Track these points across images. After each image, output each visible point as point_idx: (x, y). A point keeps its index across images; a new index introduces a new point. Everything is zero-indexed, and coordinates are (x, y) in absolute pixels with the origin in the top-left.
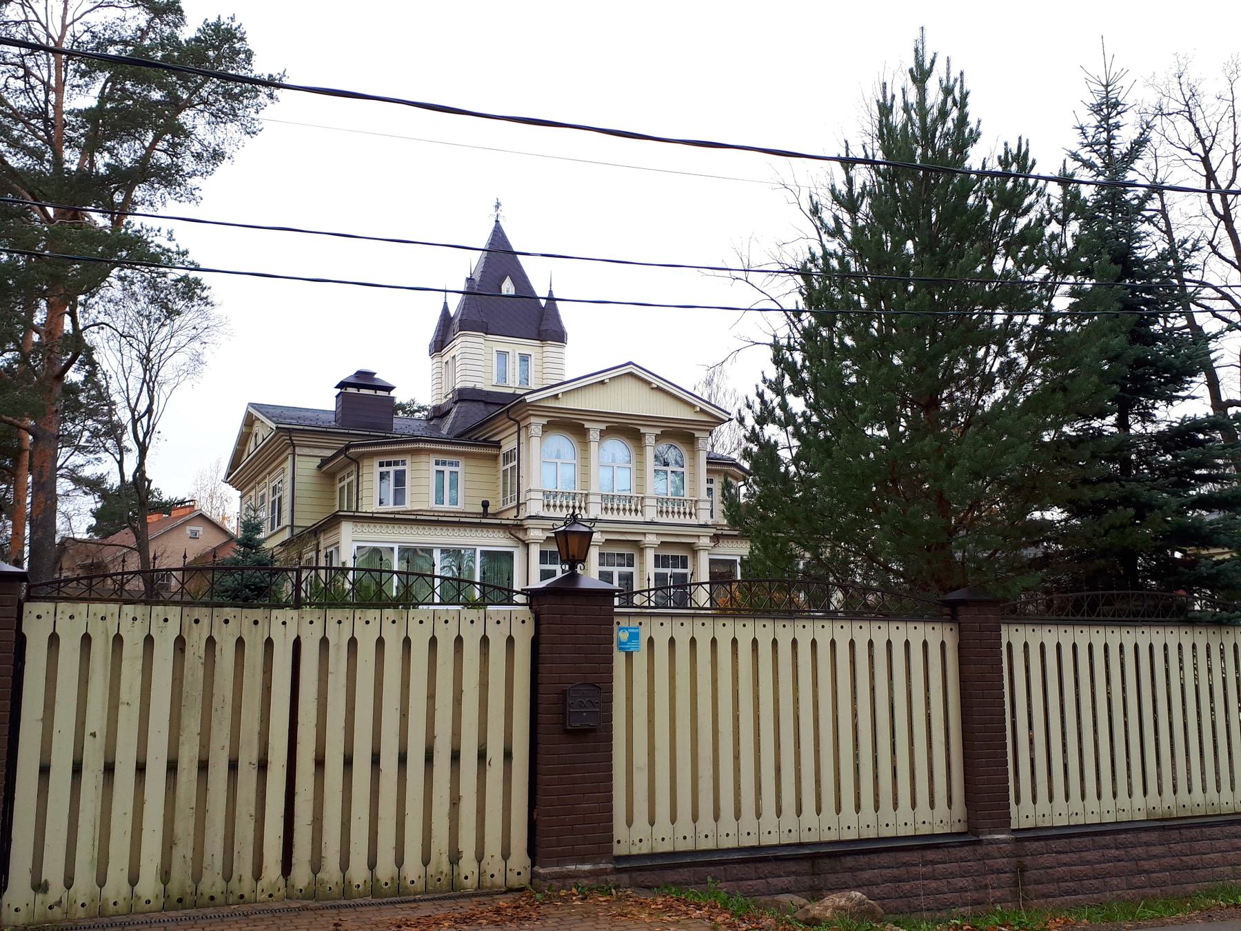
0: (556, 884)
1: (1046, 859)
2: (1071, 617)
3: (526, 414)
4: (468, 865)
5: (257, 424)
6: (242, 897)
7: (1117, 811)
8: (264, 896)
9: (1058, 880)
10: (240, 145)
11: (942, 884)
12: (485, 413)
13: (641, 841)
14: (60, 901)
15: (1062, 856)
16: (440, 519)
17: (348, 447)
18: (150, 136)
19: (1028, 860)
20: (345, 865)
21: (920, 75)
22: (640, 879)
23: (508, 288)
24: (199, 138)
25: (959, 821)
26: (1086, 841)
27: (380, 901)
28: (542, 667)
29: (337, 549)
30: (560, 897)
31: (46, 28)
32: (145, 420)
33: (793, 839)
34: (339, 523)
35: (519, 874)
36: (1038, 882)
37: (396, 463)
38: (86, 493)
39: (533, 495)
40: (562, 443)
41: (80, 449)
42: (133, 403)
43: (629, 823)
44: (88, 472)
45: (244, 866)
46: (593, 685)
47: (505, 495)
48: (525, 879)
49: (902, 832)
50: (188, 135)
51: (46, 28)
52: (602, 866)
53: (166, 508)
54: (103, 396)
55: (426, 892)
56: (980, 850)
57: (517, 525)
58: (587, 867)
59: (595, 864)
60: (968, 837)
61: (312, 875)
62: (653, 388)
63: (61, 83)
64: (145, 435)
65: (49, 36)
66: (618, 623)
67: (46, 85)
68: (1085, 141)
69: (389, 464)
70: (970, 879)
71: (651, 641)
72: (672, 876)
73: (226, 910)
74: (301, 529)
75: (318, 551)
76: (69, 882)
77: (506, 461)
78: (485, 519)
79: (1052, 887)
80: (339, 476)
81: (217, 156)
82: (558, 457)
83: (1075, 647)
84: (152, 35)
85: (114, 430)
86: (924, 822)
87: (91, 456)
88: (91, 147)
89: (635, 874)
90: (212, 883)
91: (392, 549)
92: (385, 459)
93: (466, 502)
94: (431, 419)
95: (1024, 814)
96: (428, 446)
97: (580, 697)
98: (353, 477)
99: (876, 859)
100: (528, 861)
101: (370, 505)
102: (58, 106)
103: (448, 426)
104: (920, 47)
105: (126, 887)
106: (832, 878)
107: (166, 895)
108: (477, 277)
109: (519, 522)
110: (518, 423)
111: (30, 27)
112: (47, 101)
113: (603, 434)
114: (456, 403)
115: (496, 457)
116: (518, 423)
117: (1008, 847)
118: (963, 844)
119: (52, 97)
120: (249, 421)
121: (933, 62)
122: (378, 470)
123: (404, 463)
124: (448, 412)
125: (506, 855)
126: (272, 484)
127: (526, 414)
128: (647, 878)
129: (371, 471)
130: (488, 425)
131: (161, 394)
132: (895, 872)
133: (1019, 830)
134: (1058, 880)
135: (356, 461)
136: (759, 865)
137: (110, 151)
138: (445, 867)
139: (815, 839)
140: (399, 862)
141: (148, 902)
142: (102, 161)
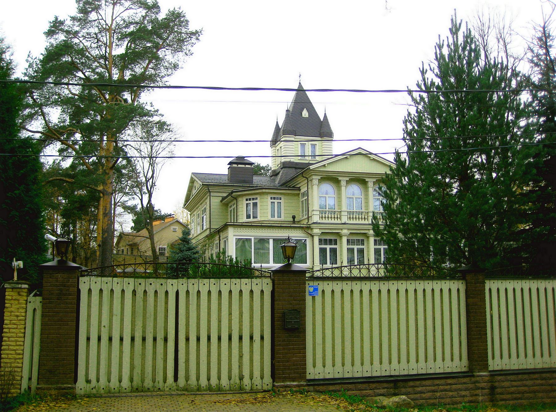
0: (281, 389)
1: (506, 384)
2: (520, 276)
3: (310, 175)
4: (246, 381)
5: (195, 182)
6: (159, 389)
7: (543, 363)
8: (167, 389)
9: (512, 393)
10: (185, 61)
11: (455, 394)
12: (295, 173)
13: (319, 373)
14: (95, 387)
15: (513, 383)
16: (272, 225)
17: (232, 192)
18: (147, 61)
19: (496, 384)
20: (198, 379)
21: (455, 30)
22: (318, 389)
23: (305, 114)
24: (167, 60)
25: (465, 367)
26: (526, 376)
27: (213, 393)
28: (276, 303)
29: (227, 239)
30: (282, 394)
31: (105, 21)
32: (151, 181)
33: (387, 374)
34: (227, 228)
35: (268, 385)
36: (501, 394)
37: (253, 199)
38: (129, 213)
39: (315, 213)
40: (328, 187)
41: (127, 194)
42: (146, 175)
43: (314, 366)
44: (130, 203)
45: (160, 377)
46: (296, 310)
47: (303, 213)
48: (270, 387)
49: (438, 371)
50: (162, 60)
51: (105, 21)
52: (302, 383)
53: (162, 218)
54: (134, 170)
55: (230, 390)
56: (473, 379)
57: (308, 227)
58: (295, 383)
59: (299, 382)
60: (469, 374)
61: (185, 382)
62: (371, 160)
63: (111, 43)
64: (151, 189)
65: (107, 24)
66: (309, 284)
67: (106, 44)
68: (534, 55)
69: (250, 200)
70: (468, 392)
71: (323, 291)
72: (331, 388)
73: (155, 393)
74: (214, 230)
75: (220, 240)
76: (98, 381)
77: (303, 197)
78: (294, 224)
79: (509, 396)
80: (230, 205)
81: (175, 67)
82: (327, 194)
83: (530, 289)
84: (147, 18)
85: (139, 185)
86: (448, 367)
87: (130, 197)
88: (122, 71)
89: (316, 387)
90: (148, 383)
91: (250, 240)
92: (248, 197)
93: (285, 217)
94: (271, 176)
95: (495, 364)
96: (267, 191)
97: (290, 315)
98: (235, 206)
99: (424, 383)
100: (272, 380)
101: (243, 219)
102: (110, 53)
103: (278, 180)
104: (454, 18)
105: (118, 383)
106: (403, 390)
107: (132, 387)
108: (291, 110)
109: (309, 226)
110: (307, 179)
111: (99, 22)
112: (106, 52)
113: (347, 182)
114: (282, 169)
115: (298, 194)
116: (307, 179)
117: (487, 378)
118: (464, 377)
119: (108, 50)
120: (192, 181)
121: (460, 24)
122: (245, 202)
123: (256, 199)
124: (279, 173)
125: (262, 378)
126: (202, 209)
127: (310, 175)
128: (321, 388)
129: (242, 204)
130: (292, 181)
131: (157, 168)
132: (433, 388)
133: (493, 371)
134: (512, 393)
135: (236, 198)
136: (370, 384)
137: (132, 69)
138: (238, 381)
139: (397, 374)
140: (219, 378)
141: (126, 389)
142: (128, 75)
